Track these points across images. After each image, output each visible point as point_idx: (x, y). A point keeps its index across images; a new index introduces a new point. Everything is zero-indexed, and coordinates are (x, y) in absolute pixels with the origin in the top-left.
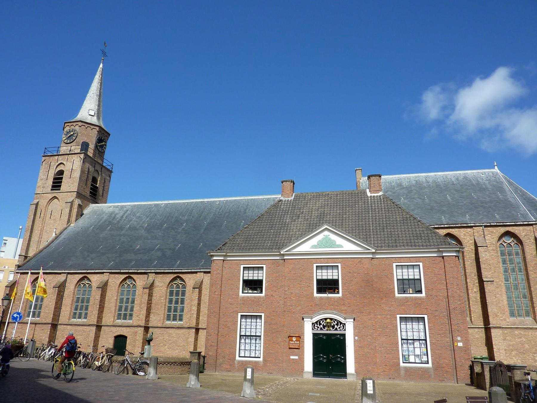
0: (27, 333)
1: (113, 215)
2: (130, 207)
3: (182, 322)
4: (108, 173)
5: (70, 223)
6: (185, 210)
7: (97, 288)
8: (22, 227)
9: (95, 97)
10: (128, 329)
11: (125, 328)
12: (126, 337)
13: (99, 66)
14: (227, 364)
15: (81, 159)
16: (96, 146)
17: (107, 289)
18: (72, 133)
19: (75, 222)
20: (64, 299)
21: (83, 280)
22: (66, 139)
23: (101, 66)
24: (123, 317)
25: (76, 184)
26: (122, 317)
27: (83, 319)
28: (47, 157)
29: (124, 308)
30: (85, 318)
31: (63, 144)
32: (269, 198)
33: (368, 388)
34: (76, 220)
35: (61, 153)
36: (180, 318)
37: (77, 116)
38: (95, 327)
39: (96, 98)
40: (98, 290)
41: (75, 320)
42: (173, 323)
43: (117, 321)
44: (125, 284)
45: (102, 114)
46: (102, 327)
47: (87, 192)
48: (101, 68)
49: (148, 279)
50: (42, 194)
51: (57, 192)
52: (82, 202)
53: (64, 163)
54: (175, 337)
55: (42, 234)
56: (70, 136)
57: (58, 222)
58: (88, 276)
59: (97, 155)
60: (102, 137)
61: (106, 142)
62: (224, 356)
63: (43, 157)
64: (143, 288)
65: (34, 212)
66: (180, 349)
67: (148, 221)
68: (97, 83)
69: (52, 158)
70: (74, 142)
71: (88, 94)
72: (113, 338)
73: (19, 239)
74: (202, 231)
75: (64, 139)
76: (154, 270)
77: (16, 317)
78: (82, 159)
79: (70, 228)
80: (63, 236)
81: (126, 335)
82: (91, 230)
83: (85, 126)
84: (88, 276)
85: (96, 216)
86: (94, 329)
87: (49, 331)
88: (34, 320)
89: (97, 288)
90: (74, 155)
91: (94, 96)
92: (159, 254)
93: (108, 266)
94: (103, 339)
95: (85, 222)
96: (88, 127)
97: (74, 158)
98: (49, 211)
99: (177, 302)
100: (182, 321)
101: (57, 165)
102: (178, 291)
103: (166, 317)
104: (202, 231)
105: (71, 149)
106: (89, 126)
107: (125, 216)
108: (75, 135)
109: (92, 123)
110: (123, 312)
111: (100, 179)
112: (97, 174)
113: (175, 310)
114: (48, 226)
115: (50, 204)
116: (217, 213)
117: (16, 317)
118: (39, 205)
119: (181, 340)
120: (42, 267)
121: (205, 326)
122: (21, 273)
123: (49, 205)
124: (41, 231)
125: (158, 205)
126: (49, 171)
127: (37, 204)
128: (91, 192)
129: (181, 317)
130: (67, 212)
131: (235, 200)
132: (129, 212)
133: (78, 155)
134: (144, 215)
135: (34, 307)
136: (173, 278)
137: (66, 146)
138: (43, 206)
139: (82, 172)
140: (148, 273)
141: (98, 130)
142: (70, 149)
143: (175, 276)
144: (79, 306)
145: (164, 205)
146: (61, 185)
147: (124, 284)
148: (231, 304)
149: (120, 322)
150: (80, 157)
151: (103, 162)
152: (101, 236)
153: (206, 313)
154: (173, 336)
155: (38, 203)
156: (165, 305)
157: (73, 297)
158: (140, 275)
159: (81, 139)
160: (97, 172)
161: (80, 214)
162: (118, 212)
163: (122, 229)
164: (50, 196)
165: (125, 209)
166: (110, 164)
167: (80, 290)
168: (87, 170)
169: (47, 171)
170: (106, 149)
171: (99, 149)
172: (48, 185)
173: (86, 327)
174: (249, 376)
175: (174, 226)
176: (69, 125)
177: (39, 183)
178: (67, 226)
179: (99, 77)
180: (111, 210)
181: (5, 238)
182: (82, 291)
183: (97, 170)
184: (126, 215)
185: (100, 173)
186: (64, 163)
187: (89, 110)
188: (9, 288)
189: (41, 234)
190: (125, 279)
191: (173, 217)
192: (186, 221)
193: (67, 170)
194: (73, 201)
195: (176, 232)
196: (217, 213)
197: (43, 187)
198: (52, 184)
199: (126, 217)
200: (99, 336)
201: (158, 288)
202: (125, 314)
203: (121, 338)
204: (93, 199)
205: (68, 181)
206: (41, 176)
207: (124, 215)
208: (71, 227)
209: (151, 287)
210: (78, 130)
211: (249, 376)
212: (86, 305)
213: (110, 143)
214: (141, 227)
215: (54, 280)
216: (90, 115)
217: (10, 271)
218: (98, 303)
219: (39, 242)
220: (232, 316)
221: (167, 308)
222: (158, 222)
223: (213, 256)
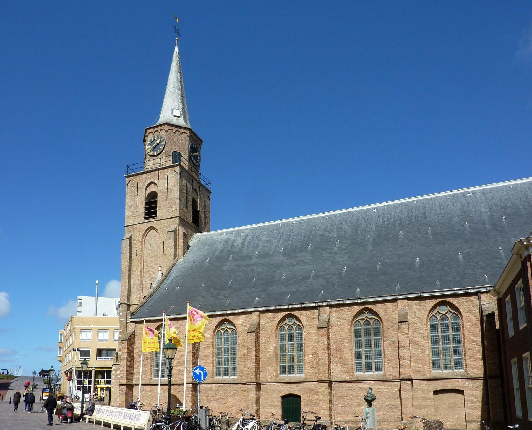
0: (185, 397)
1: (230, 243)
2: (248, 231)
4: (206, 193)
5: (177, 258)
6: (329, 225)
7: (248, 332)
8: (98, 282)
9: (177, 91)
10: (301, 386)
11: (295, 385)
12: (299, 397)
13: (174, 50)
15: (177, 173)
16: (190, 157)
17: (260, 334)
18: (158, 142)
19: (183, 256)
20: (200, 352)
21: (222, 325)
22: (151, 151)
23: (176, 49)
24: (289, 370)
25: (176, 207)
26: (287, 370)
27: (232, 376)
28: (131, 177)
29: (288, 358)
30: (234, 374)
31: (148, 158)
32: (454, 194)
34: (184, 253)
35: (147, 170)
36: (378, 367)
37: (159, 120)
38: (255, 385)
39: (178, 93)
40: (251, 335)
41: (221, 377)
42: (378, 374)
43: (281, 376)
44: (284, 325)
45: (188, 115)
46: (134, 387)
47: (189, 218)
48: (176, 52)
49: (319, 315)
50: (135, 225)
51: (153, 220)
52: (186, 231)
53: (155, 182)
55: (143, 275)
56: (156, 146)
57: (161, 258)
58: (230, 318)
59: (193, 169)
60: (194, 145)
61: (199, 152)
63: (127, 178)
64: (318, 328)
65: (128, 249)
66: (385, 409)
67: (282, 244)
68: (176, 72)
69: (138, 177)
70: (162, 153)
71: (167, 90)
72: (280, 399)
73: (97, 297)
74: (370, 248)
75: (149, 151)
76: (327, 302)
77: (198, 374)
78: (178, 173)
79: (177, 264)
80: (173, 275)
81: (298, 394)
82: (207, 264)
83: (173, 130)
84: (230, 318)
85: (207, 247)
86: (253, 387)
87: (191, 393)
88: (164, 380)
89: (248, 332)
90: (166, 170)
91: (175, 90)
94: (265, 401)
96: (176, 131)
98: (147, 247)
99: (369, 344)
101: (146, 185)
102: (368, 329)
103: (355, 366)
104: (370, 248)
105: (161, 162)
106: (177, 129)
107: (247, 242)
108: (162, 143)
109: (181, 126)
110: (287, 364)
111: (200, 201)
112: (196, 195)
113: (368, 356)
114: (149, 265)
115: (146, 236)
116: (381, 223)
117: (198, 374)
118: (133, 240)
119: (385, 397)
120: (189, 303)
121: (420, 375)
122: (136, 322)
123: (145, 238)
124: (141, 271)
125: (287, 223)
126: (137, 195)
127: (130, 239)
129: (377, 365)
130: (171, 244)
131: (401, 204)
133: (171, 168)
134: (273, 238)
135: (162, 364)
136: (358, 312)
139: (181, 190)
140: (318, 308)
141: (189, 134)
142: (159, 163)
143: (362, 308)
144: (223, 359)
145: (296, 223)
146: (156, 211)
147: (282, 326)
149: (286, 377)
150: (175, 171)
152: (224, 268)
153: (420, 357)
155: (132, 238)
156: (352, 350)
157: (213, 348)
158: (305, 312)
159: (170, 149)
160: (195, 193)
161: (187, 247)
162: (235, 239)
163: (249, 257)
164: (145, 227)
165: (243, 234)
166: (208, 183)
167: (221, 338)
168: (185, 188)
169: (135, 196)
170: (201, 161)
172: (139, 213)
173: (238, 386)
175: (323, 246)
176: (152, 132)
177: (128, 212)
178: (175, 261)
179: (177, 64)
180: (224, 238)
181: (79, 297)
182: (223, 339)
184: (247, 241)
185: (199, 193)
186: (155, 181)
187: (173, 110)
188: (126, 341)
189: (141, 276)
190: (283, 319)
192: (339, 237)
193: (161, 191)
194: (176, 229)
195: (330, 253)
196: (381, 223)
197: (133, 217)
198: (144, 211)
200: (260, 397)
201: (337, 328)
202: (291, 366)
203: (291, 398)
204: (196, 226)
205: (164, 205)
206: (128, 203)
207: (245, 241)
208: (179, 262)
209: (327, 326)
210: (165, 137)
212: (232, 357)
213: (204, 151)
216: (175, 116)
217: (98, 330)
218: (253, 353)
219: (141, 286)
221: (354, 354)
222: (297, 244)
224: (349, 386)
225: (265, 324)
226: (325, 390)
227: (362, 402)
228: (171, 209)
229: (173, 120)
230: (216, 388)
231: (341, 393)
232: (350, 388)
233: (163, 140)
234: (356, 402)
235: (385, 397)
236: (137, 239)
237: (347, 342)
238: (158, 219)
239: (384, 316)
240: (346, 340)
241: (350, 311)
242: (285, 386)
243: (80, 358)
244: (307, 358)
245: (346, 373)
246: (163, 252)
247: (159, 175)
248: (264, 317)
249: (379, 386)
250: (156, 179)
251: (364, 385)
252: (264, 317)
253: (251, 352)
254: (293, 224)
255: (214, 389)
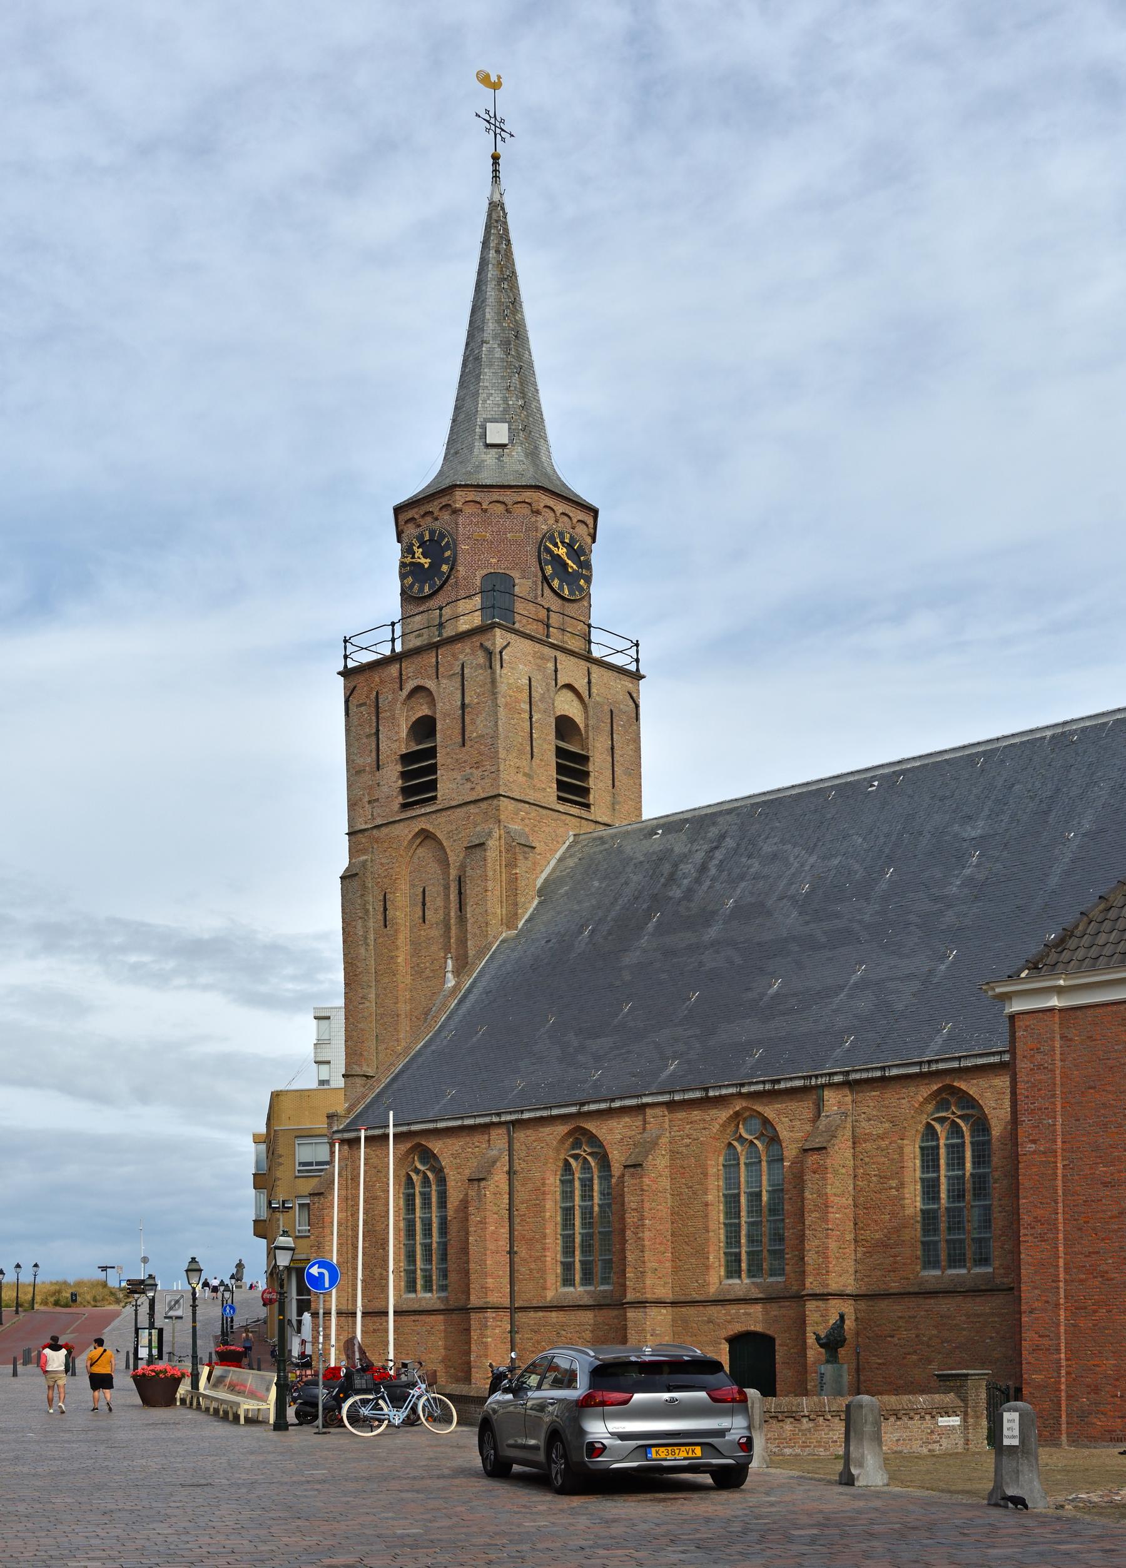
3: (990, 1270)
14: (1110, 1413)
33: (1016, 1425)
42: (977, 1275)
54: (964, 1329)
58: (591, 1126)
62: (1096, 1386)
85: (596, 884)
92: (864, 1004)
93: (660, 1080)
95: (559, 913)
97: (461, 657)
100: (990, 1265)
119: (991, 1338)
128: (561, 786)
132: (730, 843)
137: (421, 609)
138: (385, 877)
146: (435, 781)
148: (1105, 1184)
151: (590, 642)
154: (956, 1325)
162: (686, 850)
165: (713, 832)
171: (561, 587)
172: (385, 789)
174: (1014, 1437)
180: (656, 848)
183: (569, 687)
186: (430, 684)
191: (920, 833)
199: (720, 867)
207: (712, 858)
211: (1014, 1437)
214: (785, 901)
215: (469, 1155)
220: (1116, 1231)
223: (1007, 997)
224: (898, 1307)
225: (683, 1139)
226: (821, 1318)
227: (933, 1351)
228: (477, 773)
229: (483, 461)
230: (557, 1317)
231: (877, 1326)
232: (900, 1314)
233: (448, 542)
234: (915, 1352)
235: (991, 1338)
236: (386, 873)
237: (895, 1185)
238: (440, 807)
239: (994, 1109)
240: (893, 1180)
241: (902, 1095)
242: (734, 1311)
243: (299, 1171)
244: (791, 1231)
245: (889, 1271)
246: (461, 912)
247: (437, 663)
248: (681, 1120)
249: (977, 1308)
250: (429, 678)
251: (936, 1304)
252: (681, 1120)
253: (635, 1220)
254: (870, 789)
255: (554, 1320)
